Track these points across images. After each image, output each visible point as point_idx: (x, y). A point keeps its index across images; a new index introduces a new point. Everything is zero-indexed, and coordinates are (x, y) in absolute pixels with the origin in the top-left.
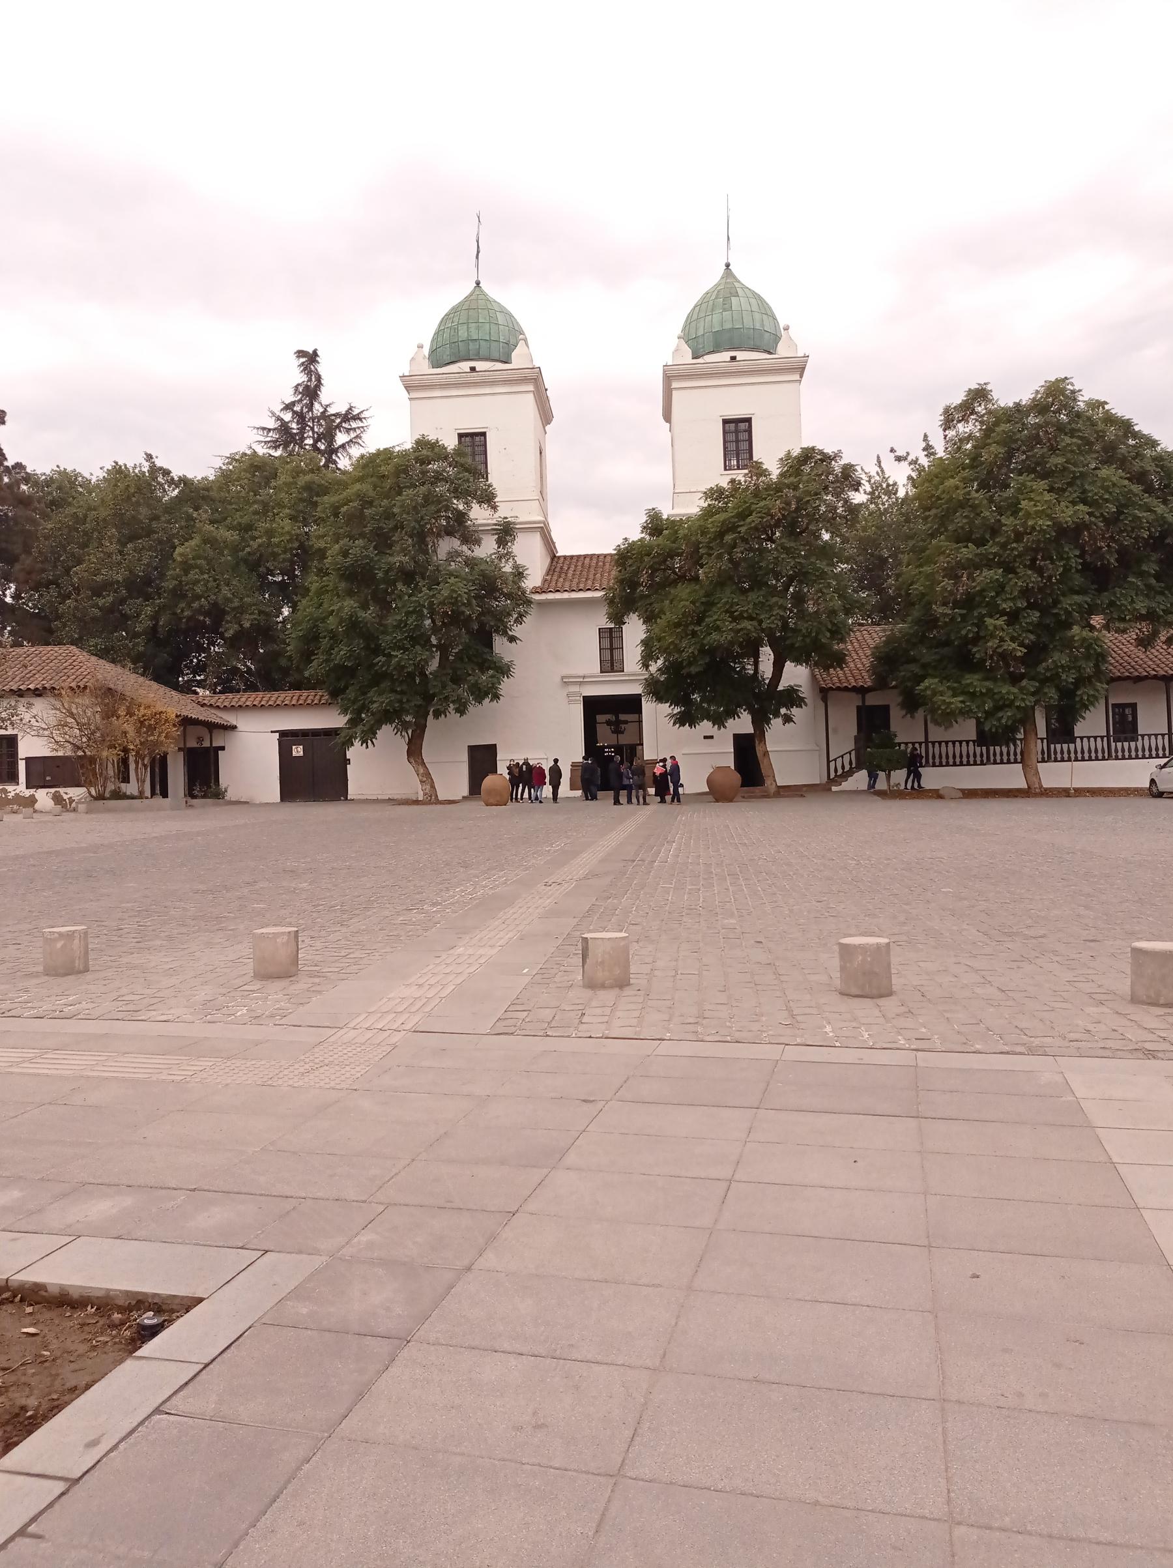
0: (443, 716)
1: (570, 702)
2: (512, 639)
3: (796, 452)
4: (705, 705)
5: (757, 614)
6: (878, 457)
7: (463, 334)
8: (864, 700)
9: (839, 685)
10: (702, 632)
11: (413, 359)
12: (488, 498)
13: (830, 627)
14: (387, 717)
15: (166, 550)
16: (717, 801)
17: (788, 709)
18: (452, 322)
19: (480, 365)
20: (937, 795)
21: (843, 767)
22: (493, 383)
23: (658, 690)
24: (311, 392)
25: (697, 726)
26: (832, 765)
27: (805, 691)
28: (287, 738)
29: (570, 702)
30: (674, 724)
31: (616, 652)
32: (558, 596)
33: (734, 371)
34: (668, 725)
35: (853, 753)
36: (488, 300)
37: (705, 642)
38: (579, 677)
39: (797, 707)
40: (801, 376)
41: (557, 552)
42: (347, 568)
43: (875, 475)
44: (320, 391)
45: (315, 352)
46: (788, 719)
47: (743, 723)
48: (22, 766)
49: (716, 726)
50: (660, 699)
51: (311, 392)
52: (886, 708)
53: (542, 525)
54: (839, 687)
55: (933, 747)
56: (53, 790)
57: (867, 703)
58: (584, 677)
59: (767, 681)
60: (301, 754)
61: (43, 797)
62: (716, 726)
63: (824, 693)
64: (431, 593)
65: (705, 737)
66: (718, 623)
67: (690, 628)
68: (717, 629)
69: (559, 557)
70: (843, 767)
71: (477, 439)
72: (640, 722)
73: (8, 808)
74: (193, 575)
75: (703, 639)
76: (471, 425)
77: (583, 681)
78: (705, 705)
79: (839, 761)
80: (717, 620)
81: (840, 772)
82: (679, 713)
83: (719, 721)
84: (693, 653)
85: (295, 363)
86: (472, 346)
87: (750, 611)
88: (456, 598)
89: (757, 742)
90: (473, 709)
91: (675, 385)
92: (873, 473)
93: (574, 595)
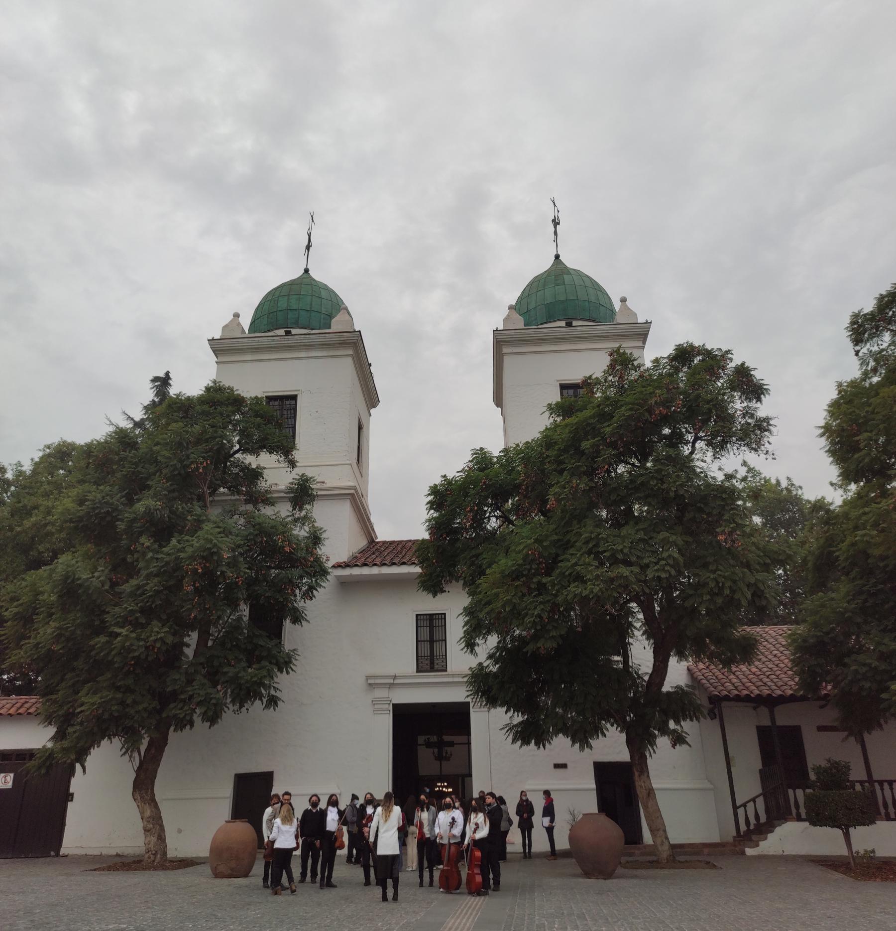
0: (188, 727)
1: (375, 712)
4: (559, 710)
5: (638, 557)
7: (283, 304)
8: (773, 719)
10: (553, 585)
16: (587, 874)
17: (677, 722)
25: (547, 745)
26: (741, 812)
29: (375, 712)
31: (437, 646)
34: (505, 744)
35: (760, 802)
37: (560, 599)
40: (644, 342)
41: (377, 538)
42: (81, 519)
45: (167, 374)
50: (492, 701)
53: (352, 491)
55: (882, 789)
57: (780, 722)
58: (395, 677)
59: (646, 678)
64: (180, 546)
65: (557, 766)
66: (578, 568)
67: (535, 580)
68: (579, 578)
69: (378, 542)
72: (469, 743)
75: (556, 596)
78: (559, 710)
79: (750, 806)
80: (576, 564)
82: (522, 723)
84: (539, 616)
87: (626, 551)
89: (637, 774)
91: (505, 350)
93: (386, 570)
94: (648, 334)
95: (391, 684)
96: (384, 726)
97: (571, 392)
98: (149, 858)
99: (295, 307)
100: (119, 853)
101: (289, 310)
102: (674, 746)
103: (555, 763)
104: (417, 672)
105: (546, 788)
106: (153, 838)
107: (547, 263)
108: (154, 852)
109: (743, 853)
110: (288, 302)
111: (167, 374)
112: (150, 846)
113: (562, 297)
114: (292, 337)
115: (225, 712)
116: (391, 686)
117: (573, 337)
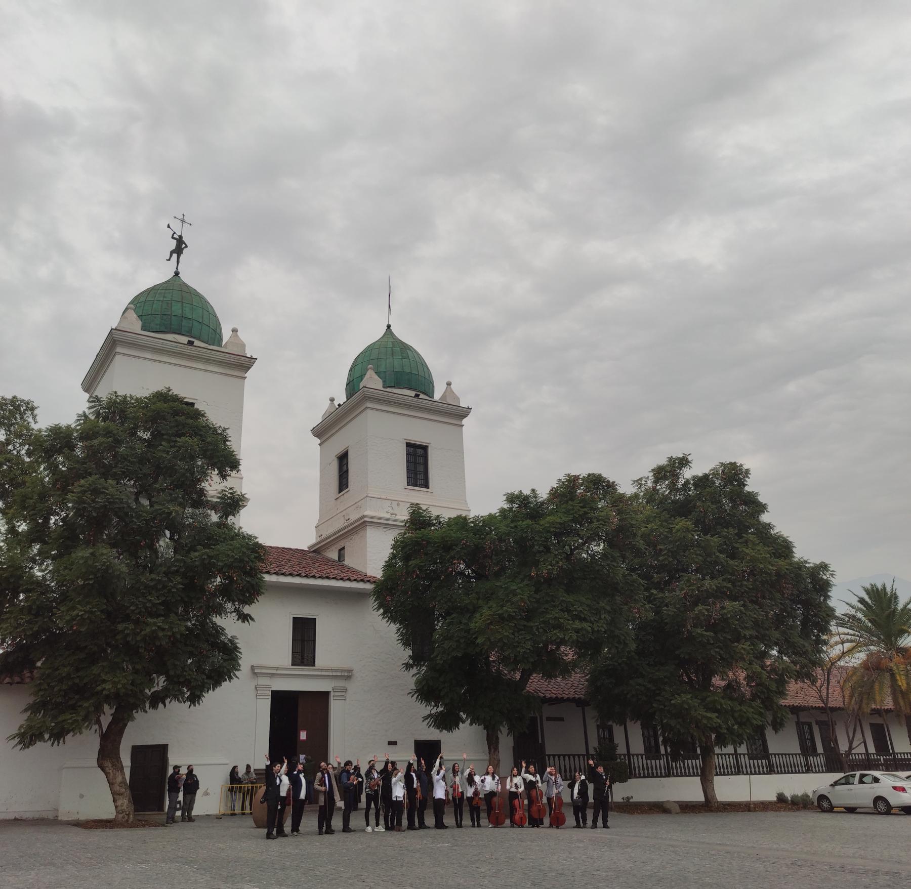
20: (630, 808)
58: (277, 669)
65: (390, 743)
86: (185, 322)
94: (250, 368)
95: (273, 674)
96: (265, 706)
97: (412, 449)
98: (123, 817)
99: (189, 316)
100: (17, 817)
101: (183, 317)
103: (389, 740)
104: (292, 665)
106: (126, 801)
107: (378, 333)
108: (127, 813)
110: (182, 309)
112: (123, 808)
114: (419, 400)
115: (786, 722)
116: (272, 675)
117: (174, 352)
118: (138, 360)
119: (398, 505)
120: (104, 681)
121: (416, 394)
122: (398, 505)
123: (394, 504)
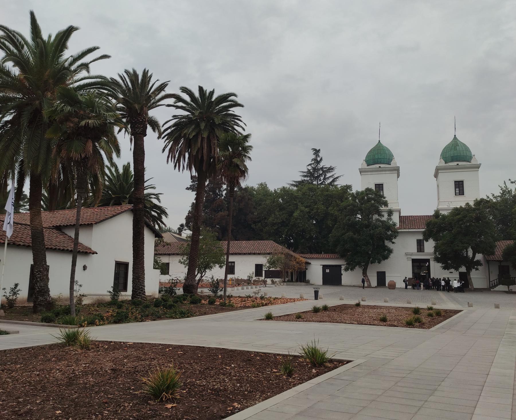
0: (373, 263)
2: (393, 243)
3: (479, 199)
4: (452, 264)
6: (504, 181)
7: (376, 157)
8: (501, 264)
9: (492, 259)
11: (362, 164)
12: (386, 204)
13: (489, 246)
14: (359, 264)
15: (291, 214)
18: (373, 153)
19: (382, 166)
21: (494, 284)
22: (385, 171)
23: (437, 260)
24: (317, 162)
26: (491, 283)
27: (482, 262)
28: (325, 267)
30: (443, 269)
32: (405, 230)
33: (458, 168)
35: (498, 279)
36: (383, 147)
37: (454, 249)
38: (411, 253)
39: (480, 266)
43: (504, 187)
44: (321, 161)
45: (319, 150)
46: (477, 269)
47: (463, 269)
48: (264, 272)
49: (456, 271)
51: (317, 162)
52: (508, 266)
54: (492, 260)
56: (271, 279)
57: (502, 265)
58: (412, 253)
59: (471, 258)
60: (329, 271)
61: (269, 281)
62: (456, 271)
63: (488, 262)
70: (494, 284)
71: (380, 185)
73: (260, 283)
74: (298, 221)
76: (379, 182)
77: (412, 254)
78: (452, 264)
81: (493, 285)
83: (457, 269)
84: (450, 251)
85: (312, 152)
88: (381, 233)
90: (383, 262)
92: (503, 187)
101: (378, 159)
102: (476, 271)
104: (417, 252)
105: (448, 277)
109: (491, 290)
111: (319, 150)
113: (456, 155)
116: (411, 255)
118: (367, 175)
119: (451, 202)
120: (356, 259)
121: (126, 265)
122: (451, 202)
123: (450, 203)
